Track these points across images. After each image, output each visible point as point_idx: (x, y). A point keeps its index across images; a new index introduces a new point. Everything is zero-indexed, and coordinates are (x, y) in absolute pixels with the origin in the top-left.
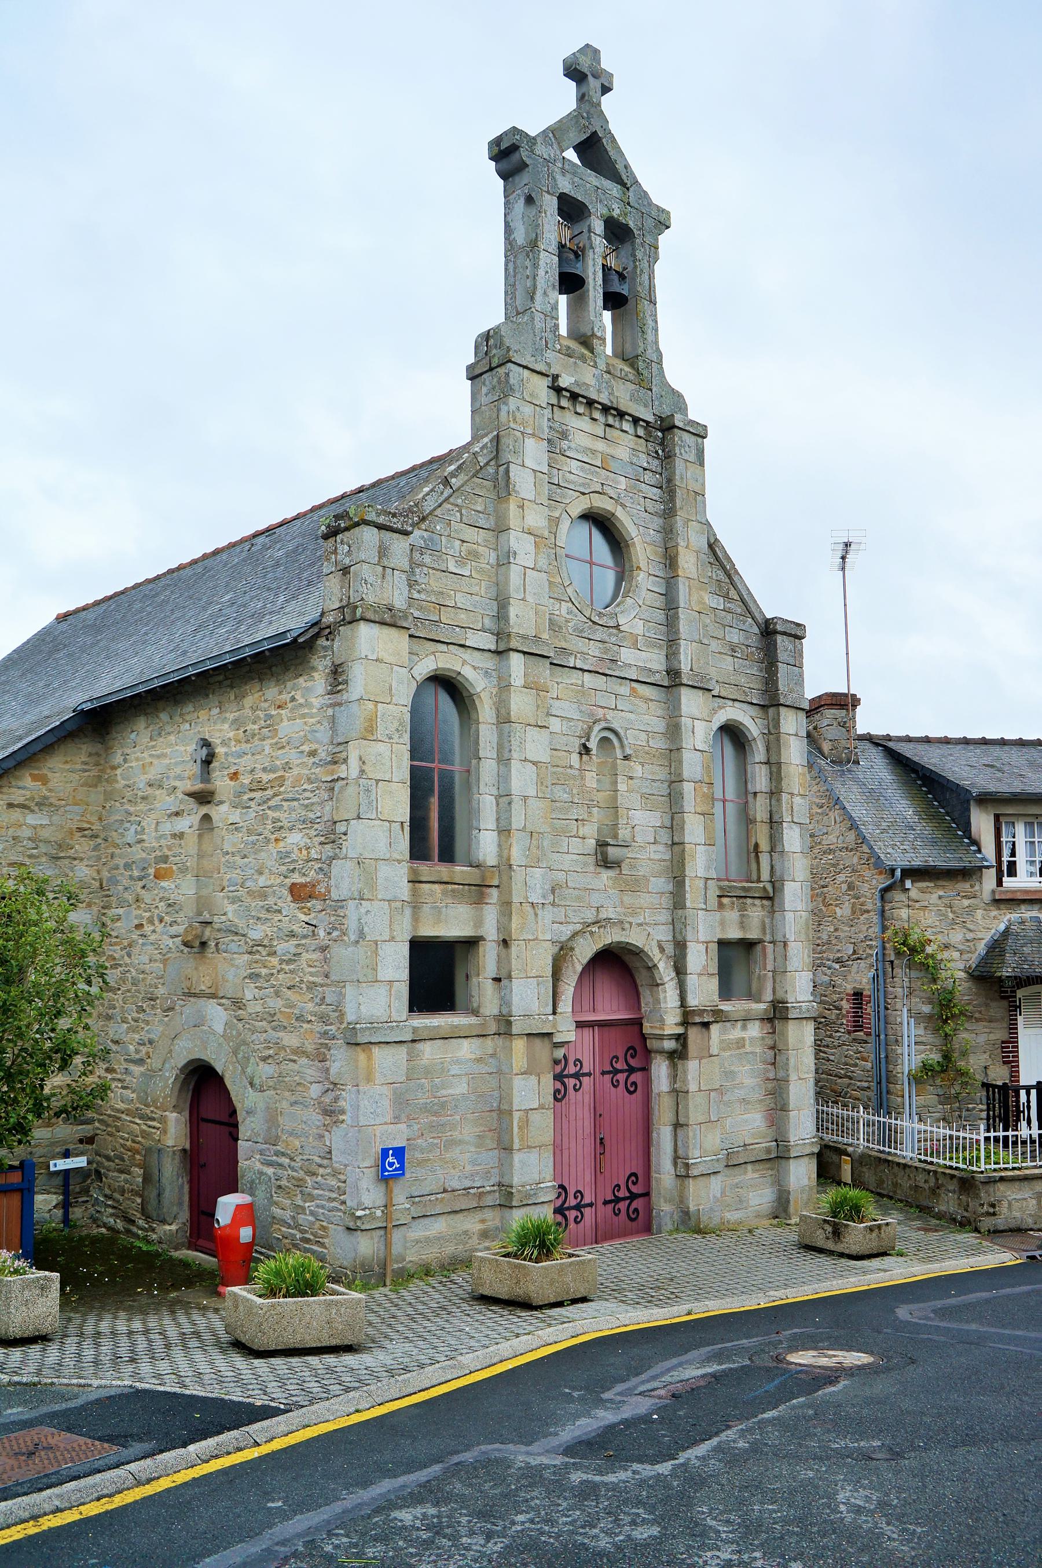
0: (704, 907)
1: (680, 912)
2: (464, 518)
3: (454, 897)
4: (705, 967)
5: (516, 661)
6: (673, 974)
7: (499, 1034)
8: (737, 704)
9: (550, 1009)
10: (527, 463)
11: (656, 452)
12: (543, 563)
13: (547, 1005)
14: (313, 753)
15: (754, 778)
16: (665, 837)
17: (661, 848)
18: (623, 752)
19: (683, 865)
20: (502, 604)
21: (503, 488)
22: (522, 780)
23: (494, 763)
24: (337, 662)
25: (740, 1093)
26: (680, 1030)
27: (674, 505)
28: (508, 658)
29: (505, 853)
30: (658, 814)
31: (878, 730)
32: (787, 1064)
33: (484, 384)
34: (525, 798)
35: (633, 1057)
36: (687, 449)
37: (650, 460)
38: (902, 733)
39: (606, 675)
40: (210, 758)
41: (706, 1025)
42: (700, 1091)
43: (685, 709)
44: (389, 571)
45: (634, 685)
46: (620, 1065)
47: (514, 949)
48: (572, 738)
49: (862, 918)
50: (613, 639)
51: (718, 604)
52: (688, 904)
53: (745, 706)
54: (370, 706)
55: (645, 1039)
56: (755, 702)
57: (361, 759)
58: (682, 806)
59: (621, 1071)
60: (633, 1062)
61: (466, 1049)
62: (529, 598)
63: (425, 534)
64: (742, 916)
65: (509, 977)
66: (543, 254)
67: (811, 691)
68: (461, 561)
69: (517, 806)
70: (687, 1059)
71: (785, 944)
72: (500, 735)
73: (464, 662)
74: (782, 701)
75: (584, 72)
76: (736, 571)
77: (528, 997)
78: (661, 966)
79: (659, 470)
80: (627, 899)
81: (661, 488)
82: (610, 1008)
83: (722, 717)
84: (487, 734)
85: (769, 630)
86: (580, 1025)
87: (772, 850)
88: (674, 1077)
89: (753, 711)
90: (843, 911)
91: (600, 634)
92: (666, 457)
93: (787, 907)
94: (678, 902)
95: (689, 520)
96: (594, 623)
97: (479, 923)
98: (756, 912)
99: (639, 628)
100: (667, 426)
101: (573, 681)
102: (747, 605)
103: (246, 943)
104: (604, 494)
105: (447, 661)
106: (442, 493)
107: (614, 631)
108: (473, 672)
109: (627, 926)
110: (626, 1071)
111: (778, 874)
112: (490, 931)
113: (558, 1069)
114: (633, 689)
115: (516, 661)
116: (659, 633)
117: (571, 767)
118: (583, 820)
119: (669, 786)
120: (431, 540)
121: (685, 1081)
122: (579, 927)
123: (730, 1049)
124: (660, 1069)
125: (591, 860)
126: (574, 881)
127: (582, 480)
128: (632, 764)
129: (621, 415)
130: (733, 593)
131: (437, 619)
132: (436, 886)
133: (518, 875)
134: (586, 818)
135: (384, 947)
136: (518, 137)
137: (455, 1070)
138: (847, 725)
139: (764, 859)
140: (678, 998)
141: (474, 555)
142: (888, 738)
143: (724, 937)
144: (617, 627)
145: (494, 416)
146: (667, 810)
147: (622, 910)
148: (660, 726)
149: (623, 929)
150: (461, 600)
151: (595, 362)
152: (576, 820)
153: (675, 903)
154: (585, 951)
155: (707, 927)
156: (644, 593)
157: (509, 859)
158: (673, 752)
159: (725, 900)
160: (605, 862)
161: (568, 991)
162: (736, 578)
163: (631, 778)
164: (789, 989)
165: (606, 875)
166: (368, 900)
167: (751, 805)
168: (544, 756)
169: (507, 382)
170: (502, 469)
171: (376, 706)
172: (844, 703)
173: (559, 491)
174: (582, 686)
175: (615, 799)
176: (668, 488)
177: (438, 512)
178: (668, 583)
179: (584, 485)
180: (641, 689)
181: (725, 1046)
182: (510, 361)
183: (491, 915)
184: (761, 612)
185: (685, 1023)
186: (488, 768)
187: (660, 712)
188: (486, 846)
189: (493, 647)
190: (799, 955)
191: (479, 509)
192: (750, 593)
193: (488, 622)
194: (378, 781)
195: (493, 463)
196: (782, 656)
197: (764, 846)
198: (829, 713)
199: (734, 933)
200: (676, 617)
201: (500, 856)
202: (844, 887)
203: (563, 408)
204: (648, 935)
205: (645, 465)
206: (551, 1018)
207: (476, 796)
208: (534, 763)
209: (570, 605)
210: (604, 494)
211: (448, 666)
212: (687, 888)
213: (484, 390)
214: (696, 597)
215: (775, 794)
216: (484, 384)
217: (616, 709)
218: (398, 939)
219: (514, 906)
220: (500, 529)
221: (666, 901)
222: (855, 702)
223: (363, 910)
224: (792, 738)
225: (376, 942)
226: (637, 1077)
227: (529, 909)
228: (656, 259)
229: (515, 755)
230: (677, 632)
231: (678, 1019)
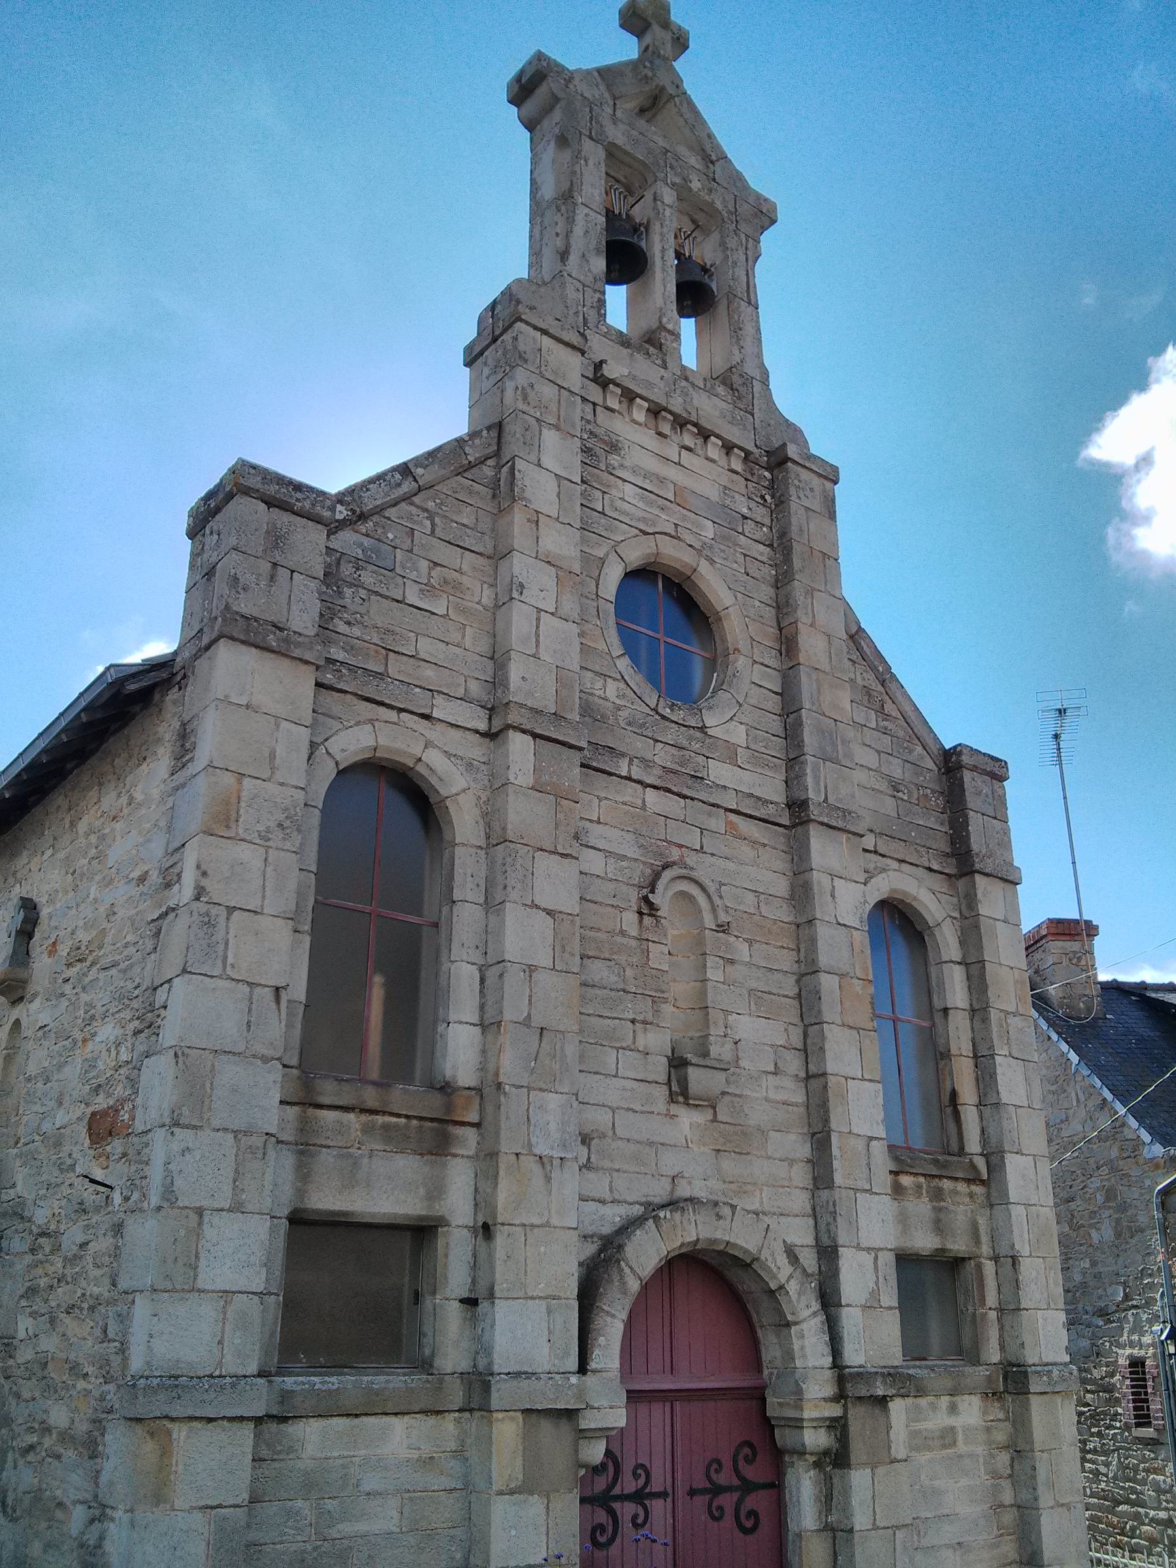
3: (388, 1140)
4: (875, 1294)
5: (519, 744)
6: (816, 1306)
7: (471, 1410)
8: (905, 867)
9: (573, 1363)
10: (547, 462)
11: (763, 497)
13: (567, 1354)
14: (142, 879)
15: (941, 984)
16: (793, 1064)
17: (788, 1083)
18: (716, 917)
19: (827, 1112)
20: (498, 659)
21: (504, 493)
23: (479, 912)
25: (949, 1533)
26: (835, 1411)
27: (791, 566)
29: (491, 1067)
32: (1034, 1477)
33: (486, 364)
34: (531, 969)
35: (749, 1461)
36: (808, 492)
37: (753, 505)
39: (685, 797)
40: (29, 927)
41: (882, 1401)
42: (875, 1528)
44: (283, 573)
45: (733, 817)
46: (724, 1478)
47: (500, 1240)
48: (624, 888)
49: (1133, 1241)
50: (696, 746)
51: (867, 719)
52: (838, 1179)
53: (921, 872)
54: (229, 779)
55: (772, 1428)
56: (935, 867)
57: (198, 867)
58: (819, 1011)
60: (750, 1472)
62: (544, 655)
63: (366, 542)
64: (938, 1210)
65: (491, 1296)
66: (581, 212)
68: (428, 589)
69: (514, 980)
71: (1015, 1260)
73: (428, 745)
74: (977, 866)
76: (893, 676)
77: (528, 1334)
78: (793, 1287)
79: (767, 521)
80: (728, 1165)
81: (770, 546)
82: (703, 1364)
83: (881, 887)
85: (952, 763)
86: (634, 1397)
88: (828, 1499)
89: (937, 883)
90: (1105, 1233)
91: (671, 734)
92: (778, 502)
93: (1013, 1196)
94: (821, 1175)
95: (813, 589)
96: (663, 717)
97: (436, 1191)
98: (963, 1205)
99: (738, 735)
100: (778, 460)
102: (911, 728)
103: (31, 1232)
104: (679, 539)
105: (399, 740)
106: (399, 485)
107: (698, 734)
108: (446, 762)
109: (726, 1211)
110: (737, 1488)
111: (993, 1141)
112: (458, 1206)
113: (601, 1484)
115: (519, 744)
116: (776, 747)
117: (623, 933)
118: (645, 1022)
119: (798, 981)
120: (377, 552)
121: (846, 1510)
122: (638, 1210)
123: (929, 1449)
124: (804, 1486)
125: (661, 1093)
126: (628, 1125)
127: (641, 514)
130: (889, 707)
131: (380, 669)
132: (351, 1116)
133: (513, 1105)
134: (650, 1018)
137: (371, 1482)
138: (1084, 960)
139: (970, 1116)
140: (827, 1350)
141: (452, 587)
143: (909, 1244)
144: (703, 729)
146: (797, 1020)
147: (720, 1186)
148: (781, 886)
149: (719, 1217)
150: (425, 647)
151: (664, 362)
152: (633, 1021)
153: (814, 1179)
154: (646, 1253)
155: (878, 1226)
156: (745, 686)
157: (497, 1074)
158: (804, 927)
159: (906, 1180)
160: (680, 1092)
163: (732, 962)
164: (1027, 1338)
165: (688, 1120)
167: (940, 1028)
169: (515, 348)
170: (505, 469)
171: (240, 782)
172: (1074, 932)
173: (603, 521)
175: (703, 993)
176: (782, 545)
177: (392, 513)
179: (644, 520)
181: (919, 1441)
182: (520, 319)
184: (936, 739)
185: (840, 1396)
186: (466, 920)
188: (459, 1052)
189: (482, 726)
190: (1041, 1283)
191: (465, 521)
193: (475, 688)
194: (231, 910)
195: (490, 462)
196: (972, 801)
198: (1056, 946)
199: (924, 1242)
200: (799, 724)
202: (1100, 1198)
203: (612, 410)
205: (745, 511)
206: (574, 1380)
207: (444, 968)
208: (549, 913)
209: (622, 685)
210: (679, 539)
211: (398, 745)
212: (835, 1151)
213: (486, 371)
214: (831, 700)
215: (979, 1011)
216: (486, 364)
218: (250, 1208)
220: (499, 556)
221: (801, 1175)
222: (1090, 930)
223: (176, 1147)
225: (200, 1212)
226: (758, 1501)
227: (536, 1168)
229: (514, 895)
230: (800, 745)
231: (829, 1390)
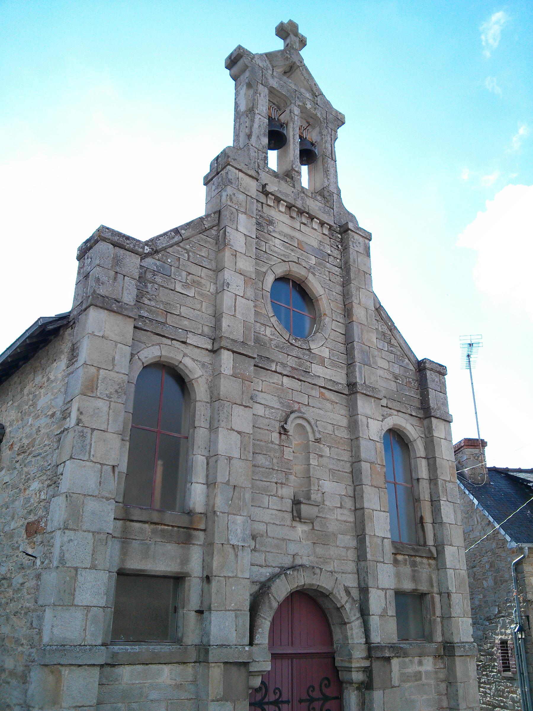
0: (382, 560)
1: (362, 563)
2: (191, 258)
4: (385, 610)
5: (226, 357)
6: (358, 615)
7: (200, 662)
8: (400, 414)
9: (247, 640)
10: (241, 229)
11: (337, 246)
12: (250, 293)
14: (53, 415)
16: (349, 504)
18: (314, 436)
20: (217, 316)
22: (227, 443)
23: (207, 432)
24: (75, 342)
26: (366, 664)
28: (220, 355)
30: (343, 486)
31: (501, 464)
32: (457, 695)
33: (213, 184)
34: (230, 459)
36: (357, 244)
37: (333, 249)
38: (517, 467)
39: (301, 381)
43: (360, 410)
45: (323, 390)
46: (316, 694)
47: (214, 584)
48: (273, 422)
49: (502, 586)
52: (369, 556)
53: (407, 416)
55: (338, 671)
56: (414, 414)
57: (78, 410)
58: (361, 480)
59: (318, 700)
61: (166, 675)
62: (238, 315)
63: (158, 263)
65: (210, 609)
67: (456, 439)
68: (186, 285)
69: (222, 463)
70: (373, 689)
72: (213, 410)
73: (185, 355)
74: (433, 414)
75: (286, 31)
76: (395, 327)
77: (226, 627)
78: (348, 606)
79: (339, 257)
80: (319, 550)
81: (341, 268)
82: (306, 643)
83: (389, 423)
84: (202, 412)
85: (422, 367)
86: (275, 657)
87: (433, 523)
89: (415, 421)
91: (295, 352)
95: (360, 288)
96: (292, 344)
97: (185, 560)
98: (425, 568)
99: (326, 353)
100: (344, 230)
101: (275, 381)
104: (299, 264)
107: (307, 352)
108: (193, 364)
109: (318, 571)
113: (259, 697)
114: (322, 394)
115: (226, 357)
117: (272, 442)
118: (281, 484)
119: (351, 465)
120: (163, 268)
122: (277, 570)
127: (283, 253)
128: (322, 446)
129: (312, 218)
130: (393, 341)
132: (147, 526)
133: (221, 520)
134: (284, 481)
135: (84, 573)
136: (242, 51)
137: (153, 695)
138: (480, 457)
139: (429, 528)
141: (196, 284)
142: (507, 470)
144: (309, 350)
145: (219, 201)
146: (351, 483)
148: (344, 422)
149: (314, 574)
150: (184, 311)
151: (294, 185)
152: (276, 483)
153: (358, 556)
154: (281, 590)
155: (386, 578)
156: (329, 331)
159: (400, 557)
161: (265, 625)
162: (395, 332)
163: (322, 456)
165: (301, 529)
166: (71, 530)
168: (248, 429)
170: (221, 231)
171: (98, 371)
172: (476, 445)
174: (282, 385)
175: (308, 470)
177: (170, 250)
178: (346, 327)
179: (284, 255)
180: (327, 393)
181: (405, 678)
183: (196, 556)
184: (414, 356)
185: (369, 657)
186: (201, 435)
187: (343, 412)
188: (197, 495)
189: (210, 347)
191: (203, 255)
192: (406, 342)
193: (206, 330)
194: (93, 430)
195: (215, 228)
196: (430, 384)
197: (428, 519)
199: (408, 586)
200: (353, 348)
201: (207, 504)
202: (487, 566)
204: (336, 578)
205: (329, 252)
206: (247, 648)
207: (190, 458)
208: (239, 433)
209: (273, 330)
210: (299, 264)
211: (171, 355)
212: (368, 544)
213: (214, 187)
217: (308, 405)
219: (216, 546)
220: (218, 270)
221: (352, 555)
222: (483, 444)
223: (66, 539)
224: (442, 441)
225: (76, 569)
227: (231, 550)
228: (336, 139)
229: (223, 424)
230: (353, 358)
231: (364, 654)
